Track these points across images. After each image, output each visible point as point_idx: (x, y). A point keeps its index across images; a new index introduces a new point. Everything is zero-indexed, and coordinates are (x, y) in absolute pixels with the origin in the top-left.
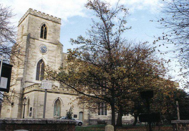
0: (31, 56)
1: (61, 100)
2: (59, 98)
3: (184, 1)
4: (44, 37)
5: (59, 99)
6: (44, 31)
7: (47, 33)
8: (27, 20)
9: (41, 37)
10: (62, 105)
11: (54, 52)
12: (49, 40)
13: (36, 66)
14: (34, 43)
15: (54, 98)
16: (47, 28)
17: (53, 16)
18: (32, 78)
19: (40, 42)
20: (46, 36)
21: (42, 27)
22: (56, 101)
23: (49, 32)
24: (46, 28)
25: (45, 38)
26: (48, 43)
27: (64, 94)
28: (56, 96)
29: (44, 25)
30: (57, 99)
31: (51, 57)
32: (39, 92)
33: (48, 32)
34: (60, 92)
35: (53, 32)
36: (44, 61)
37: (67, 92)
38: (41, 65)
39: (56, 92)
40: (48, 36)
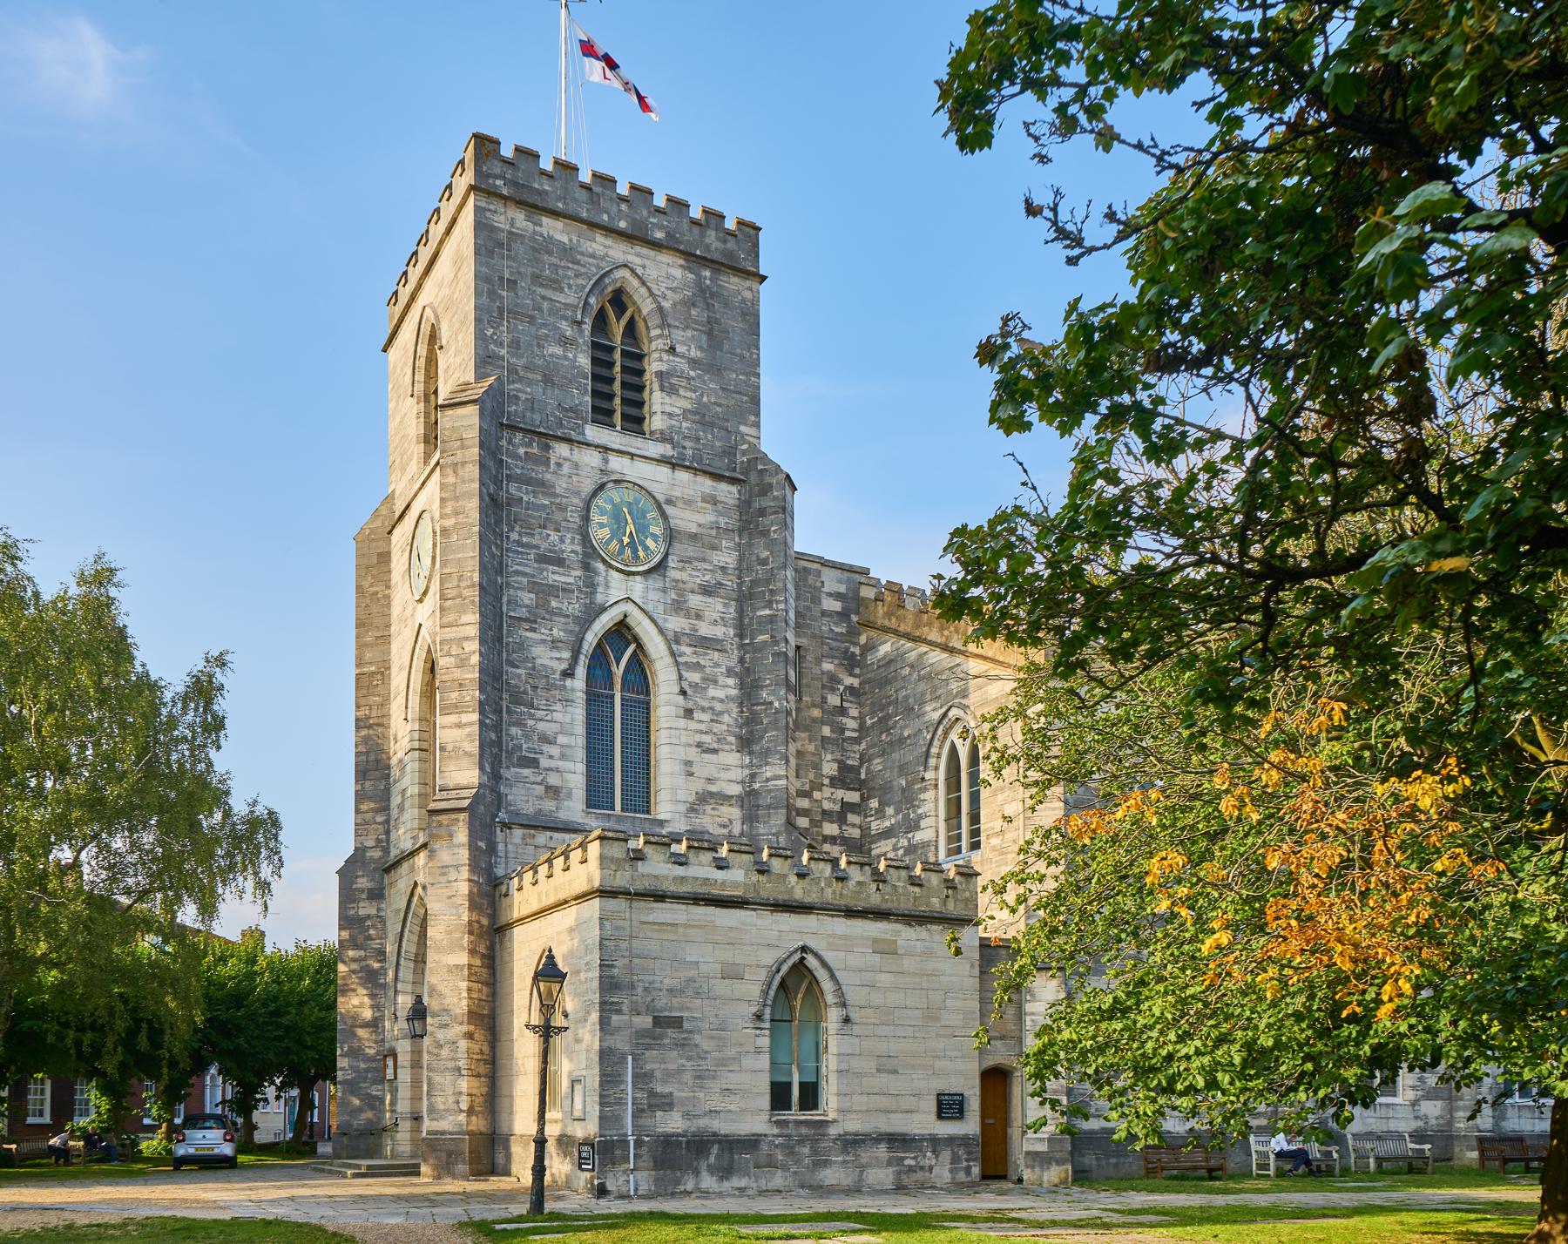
0: (527, 598)
1: (821, 974)
2: (804, 949)
3: (721, 1239)
4: (624, 417)
5: (811, 961)
6: (617, 356)
7: (641, 373)
8: (457, 261)
9: (602, 415)
10: (833, 1016)
11: (714, 548)
12: (664, 438)
13: (579, 683)
14: (540, 473)
15: (769, 958)
16: (641, 325)
17: (536, 156)
18: (554, 792)
19: (591, 458)
20: (640, 404)
21: (600, 322)
22: (782, 984)
23: (664, 367)
24: (631, 330)
25: (635, 422)
26: (664, 471)
27: (850, 913)
28: (790, 931)
29: (619, 300)
30: (794, 966)
31: (695, 601)
32: (639, 904)
33: (653, 366)
34: (812, 898)
35: (694, 363)
36: (645, 640)
37: (874, 899)
38: (618, 671)
39: (781, 897)
40: (660, 407)
